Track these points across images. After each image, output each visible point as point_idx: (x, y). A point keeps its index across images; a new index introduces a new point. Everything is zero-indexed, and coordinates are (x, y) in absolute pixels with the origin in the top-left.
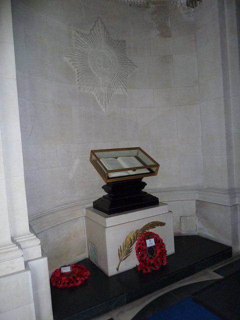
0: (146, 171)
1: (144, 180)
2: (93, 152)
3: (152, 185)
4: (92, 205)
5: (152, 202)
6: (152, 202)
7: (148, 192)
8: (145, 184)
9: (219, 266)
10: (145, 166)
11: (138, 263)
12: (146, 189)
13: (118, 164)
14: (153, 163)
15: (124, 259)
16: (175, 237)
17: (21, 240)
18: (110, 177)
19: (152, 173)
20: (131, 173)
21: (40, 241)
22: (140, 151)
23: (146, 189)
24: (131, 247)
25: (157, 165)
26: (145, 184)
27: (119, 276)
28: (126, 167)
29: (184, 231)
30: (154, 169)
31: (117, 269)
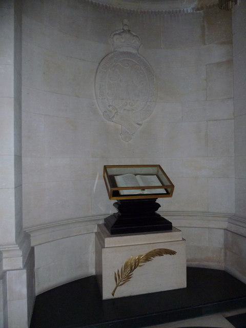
0: (163, 191)
1: (158, 201)
2: (105, 166)
3: (165, 207)
4: (102, 222)
5: (164, 226)
6: (164, 226)
7: (162, 215)
8: (159, 206)
9: (229, 314)
10: (163, 186)
11: (184, 285)
12: (159, 211)
13: (137, 182)
14: (169, 184)
15: (121, 285)
16: (189, 269)
17: (4, 249)
18: (122, 194)
19: (168, 194)
20: (146, 192)
21: (21, 253)
22: (160, 171)
23: (159, 211)
24: (130, 273)
25: (172, 186)
26: (159, 206)
27: (114, 302)
28: (142, 185)
29: (194, 264)
30: (169, 190)
31: (113, 295)
